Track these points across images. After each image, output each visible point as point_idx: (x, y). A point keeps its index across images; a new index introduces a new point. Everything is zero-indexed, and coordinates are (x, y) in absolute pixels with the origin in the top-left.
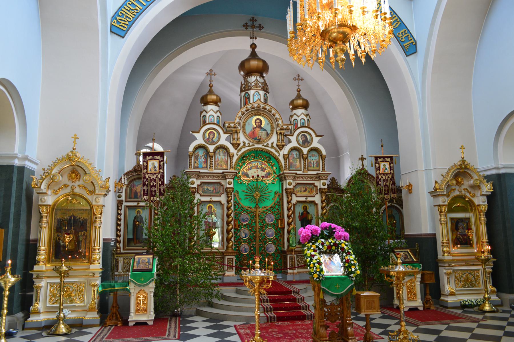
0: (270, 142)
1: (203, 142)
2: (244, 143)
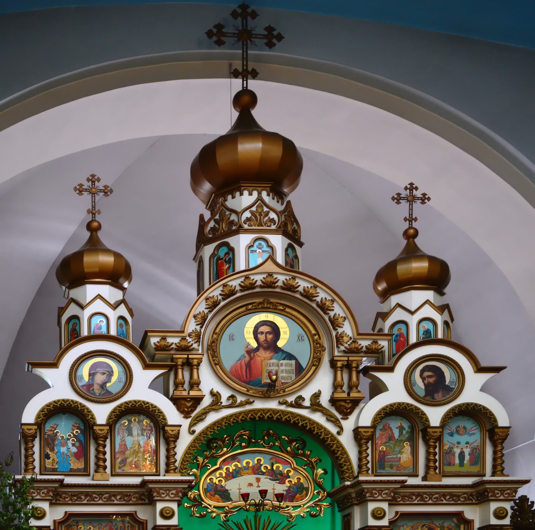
0: (307, 393)
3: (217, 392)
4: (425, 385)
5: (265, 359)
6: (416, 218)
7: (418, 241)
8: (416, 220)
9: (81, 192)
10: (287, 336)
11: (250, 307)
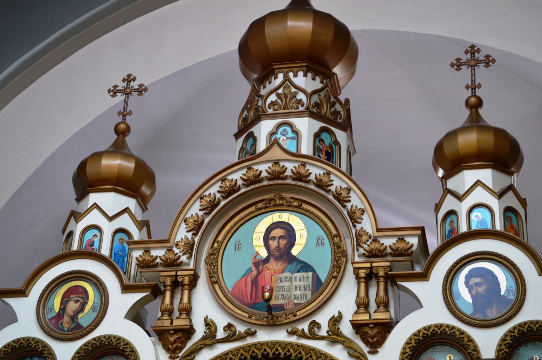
0: (323, 318)
1: (37, 333)
2: (209, 324)
3: (212, 321)
4: (472, 297)
5: (275, 273)
6: (479, 84)
7: (481, 111)
8: (479, 86)
9: (115, 93)
10: (304, 241)
11: (260, 205)
